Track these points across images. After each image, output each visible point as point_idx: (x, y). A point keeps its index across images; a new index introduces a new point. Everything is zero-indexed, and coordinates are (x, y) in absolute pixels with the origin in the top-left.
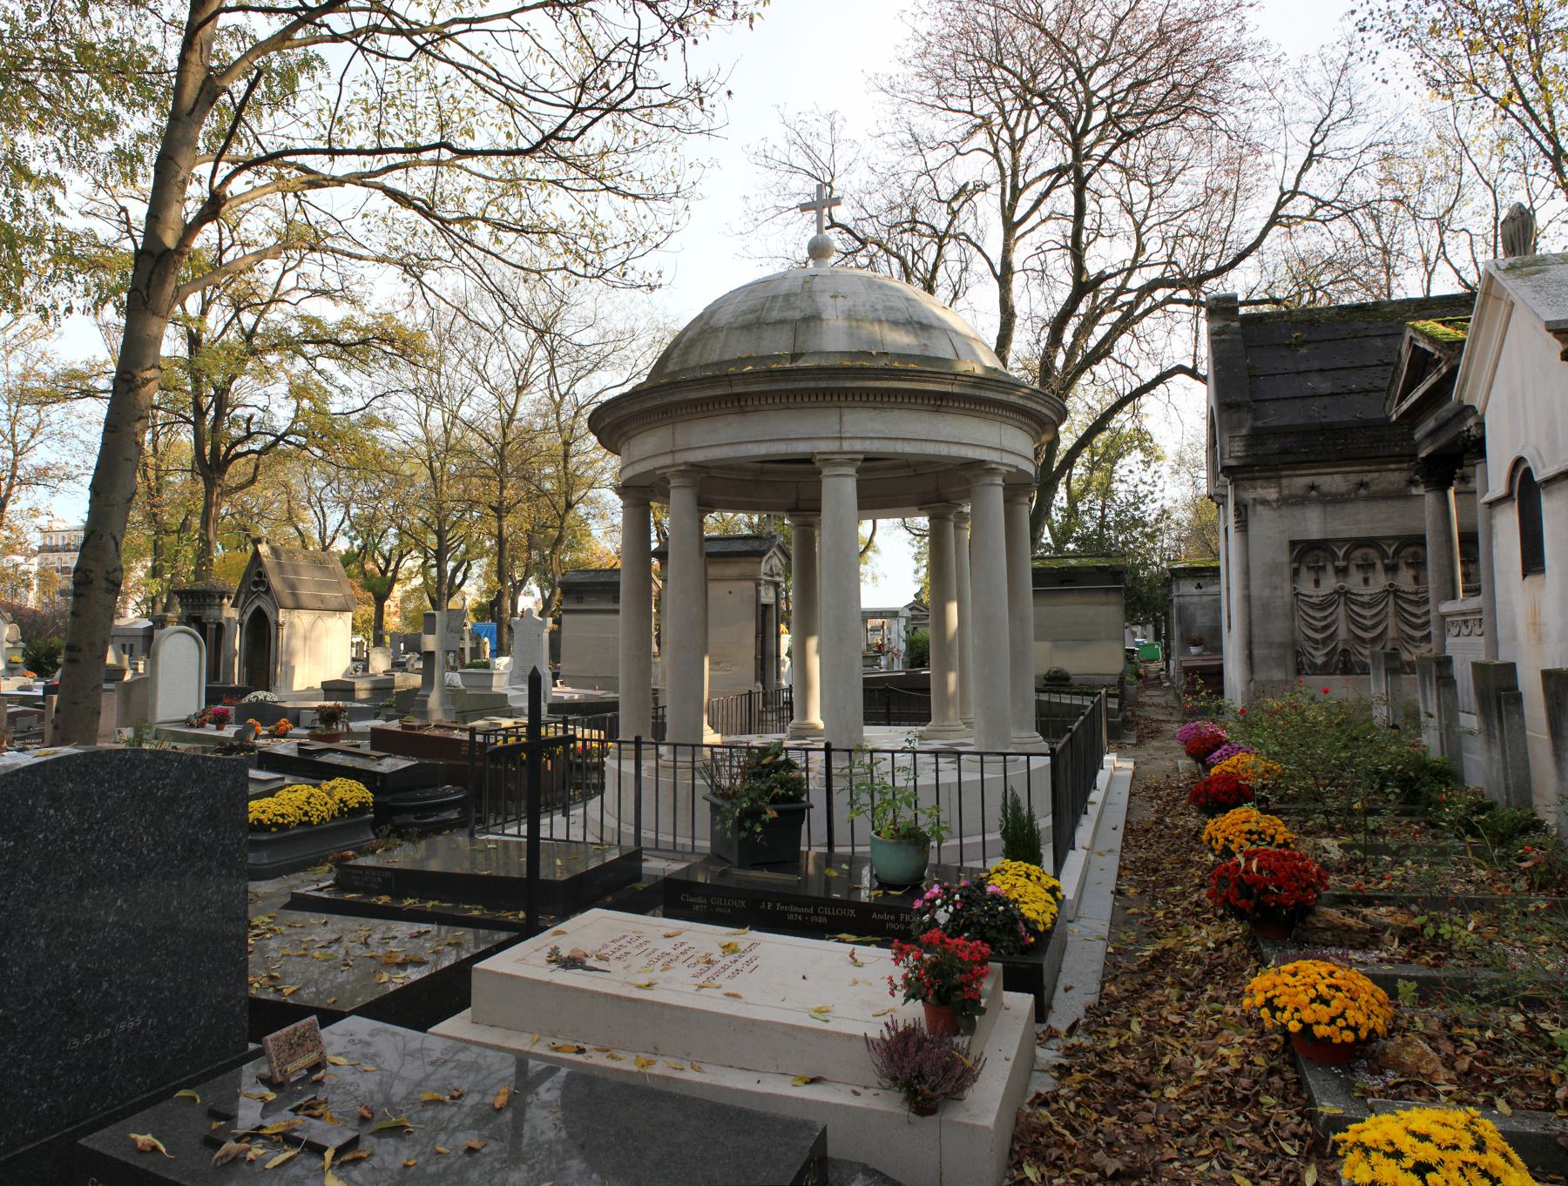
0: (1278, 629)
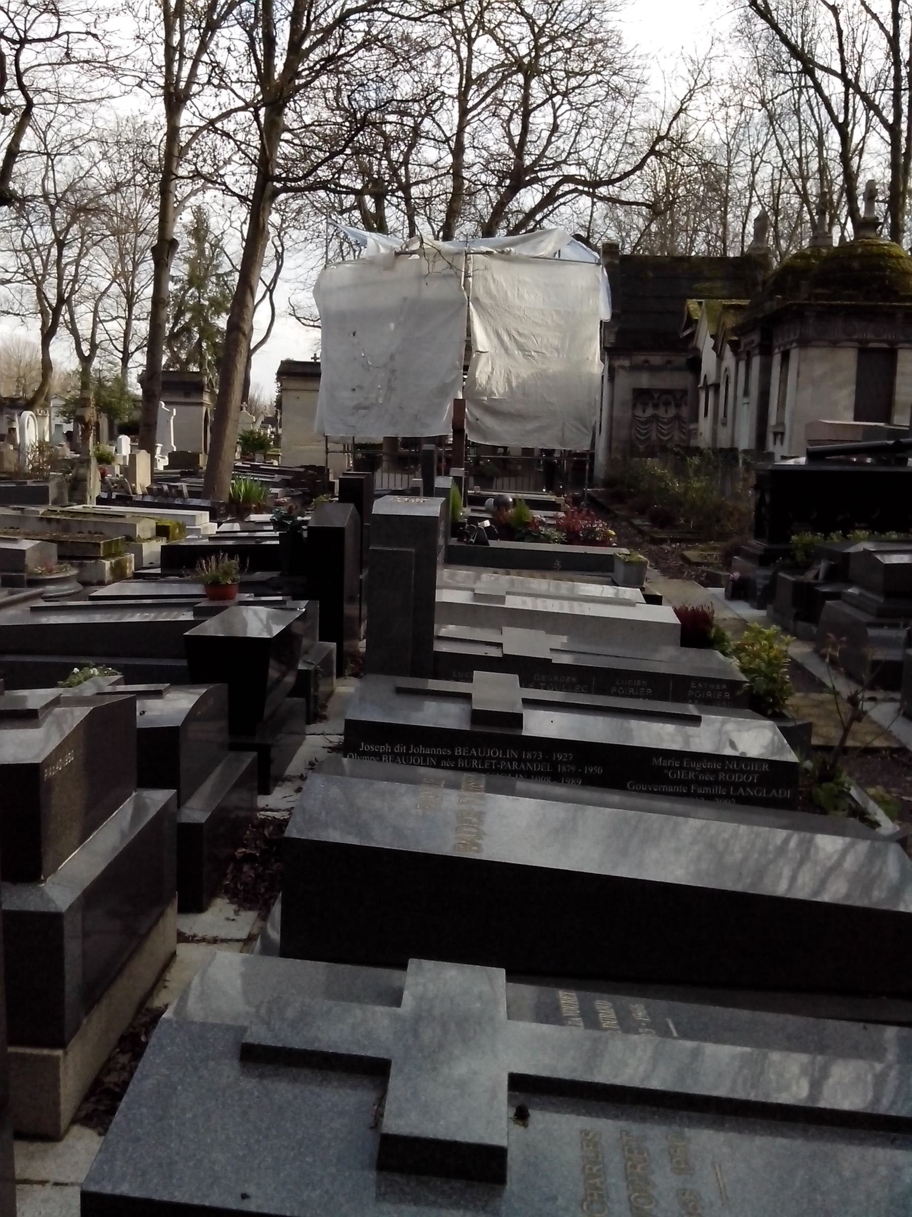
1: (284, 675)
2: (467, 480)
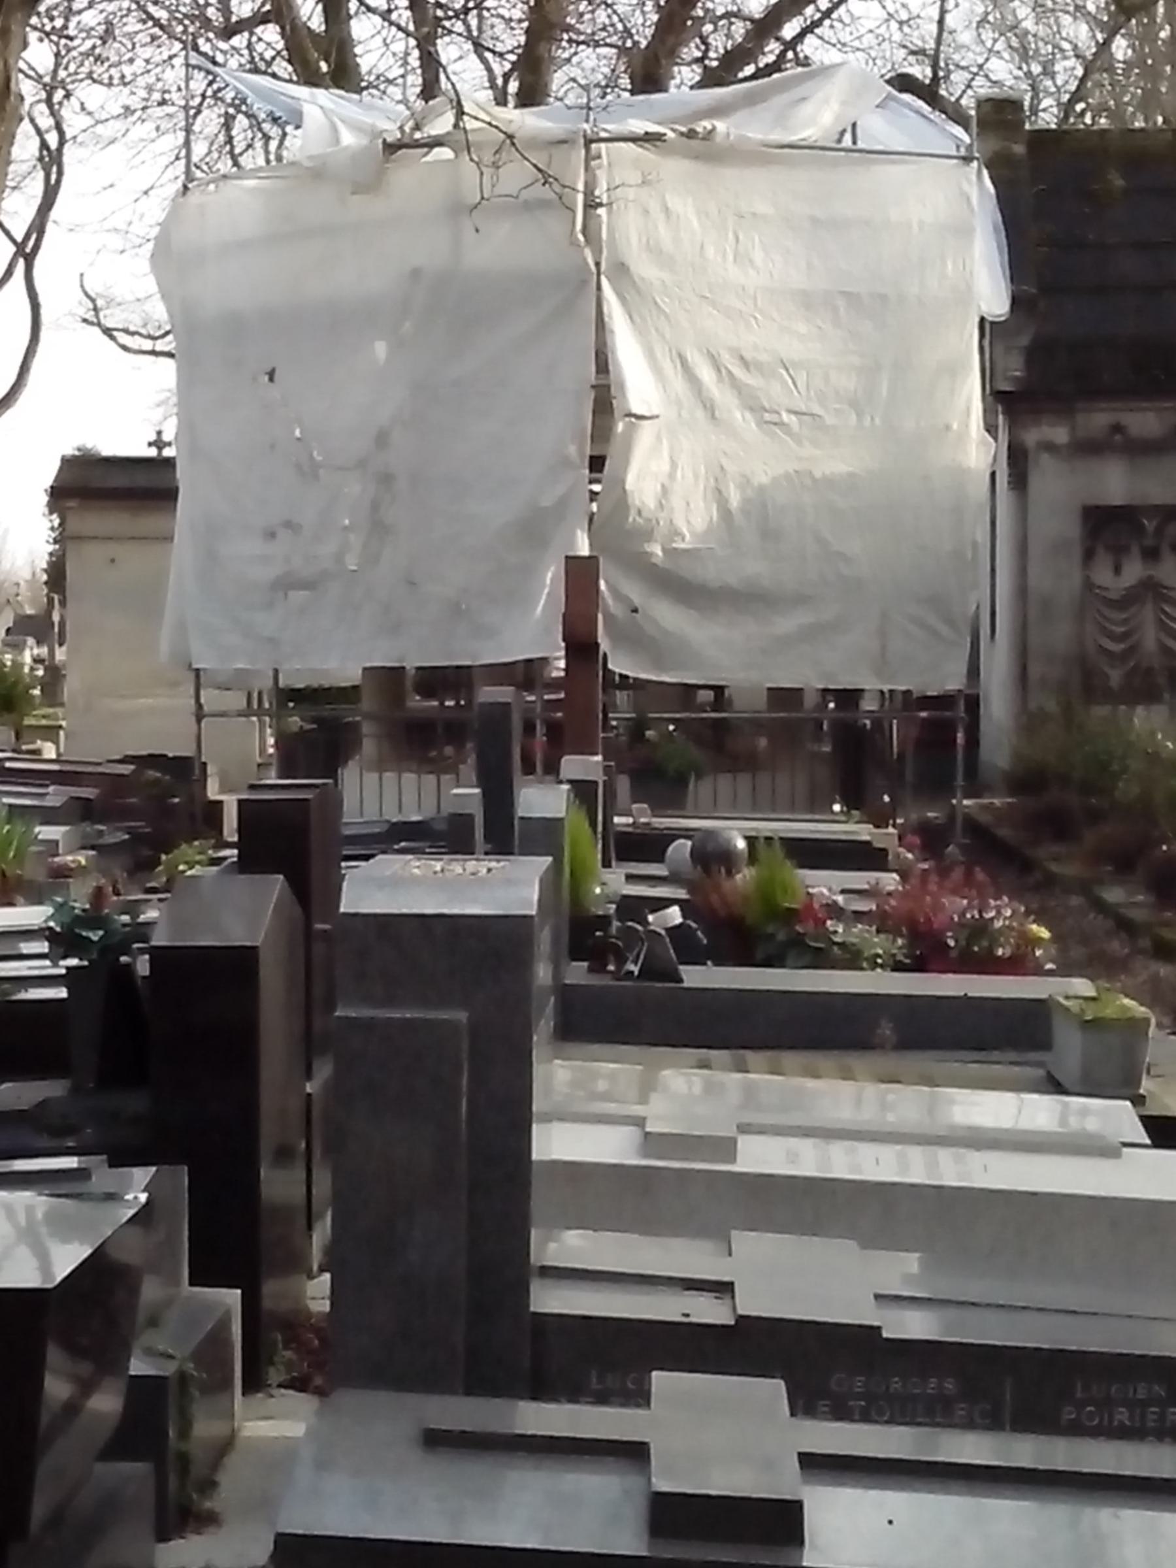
0: (1059, 635)
1: (87, 1387)
2: (610, 788)
